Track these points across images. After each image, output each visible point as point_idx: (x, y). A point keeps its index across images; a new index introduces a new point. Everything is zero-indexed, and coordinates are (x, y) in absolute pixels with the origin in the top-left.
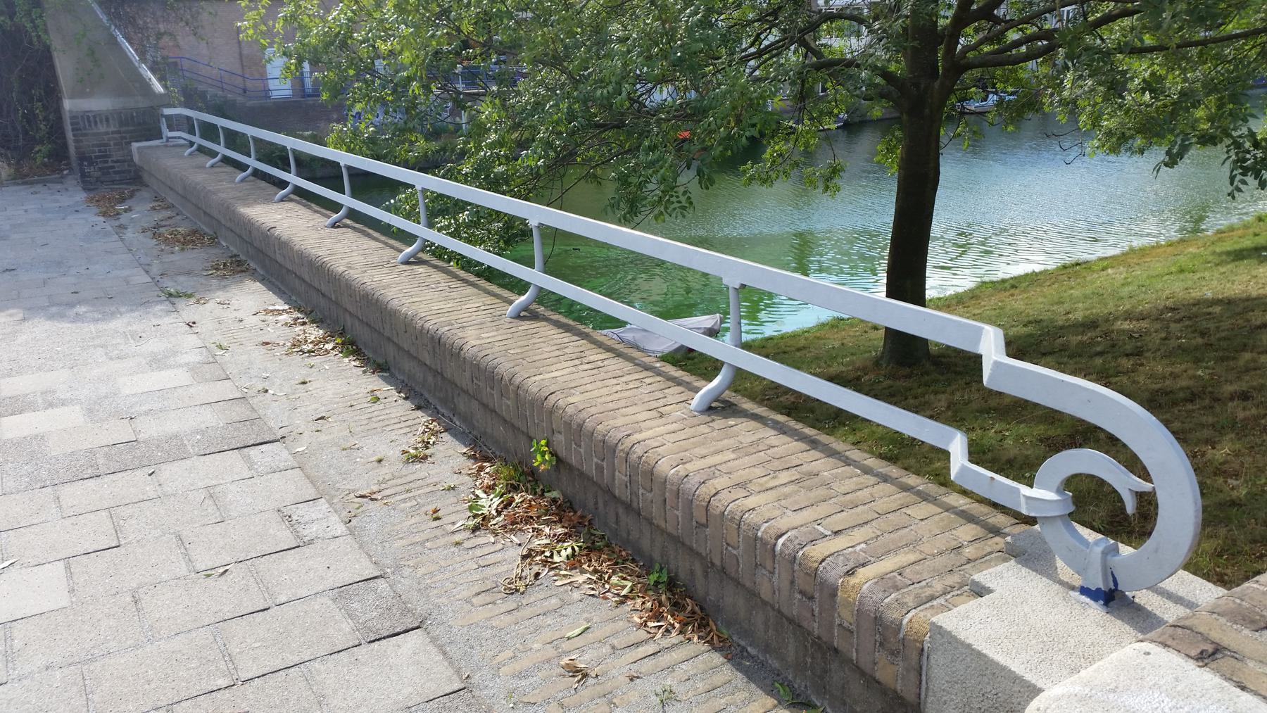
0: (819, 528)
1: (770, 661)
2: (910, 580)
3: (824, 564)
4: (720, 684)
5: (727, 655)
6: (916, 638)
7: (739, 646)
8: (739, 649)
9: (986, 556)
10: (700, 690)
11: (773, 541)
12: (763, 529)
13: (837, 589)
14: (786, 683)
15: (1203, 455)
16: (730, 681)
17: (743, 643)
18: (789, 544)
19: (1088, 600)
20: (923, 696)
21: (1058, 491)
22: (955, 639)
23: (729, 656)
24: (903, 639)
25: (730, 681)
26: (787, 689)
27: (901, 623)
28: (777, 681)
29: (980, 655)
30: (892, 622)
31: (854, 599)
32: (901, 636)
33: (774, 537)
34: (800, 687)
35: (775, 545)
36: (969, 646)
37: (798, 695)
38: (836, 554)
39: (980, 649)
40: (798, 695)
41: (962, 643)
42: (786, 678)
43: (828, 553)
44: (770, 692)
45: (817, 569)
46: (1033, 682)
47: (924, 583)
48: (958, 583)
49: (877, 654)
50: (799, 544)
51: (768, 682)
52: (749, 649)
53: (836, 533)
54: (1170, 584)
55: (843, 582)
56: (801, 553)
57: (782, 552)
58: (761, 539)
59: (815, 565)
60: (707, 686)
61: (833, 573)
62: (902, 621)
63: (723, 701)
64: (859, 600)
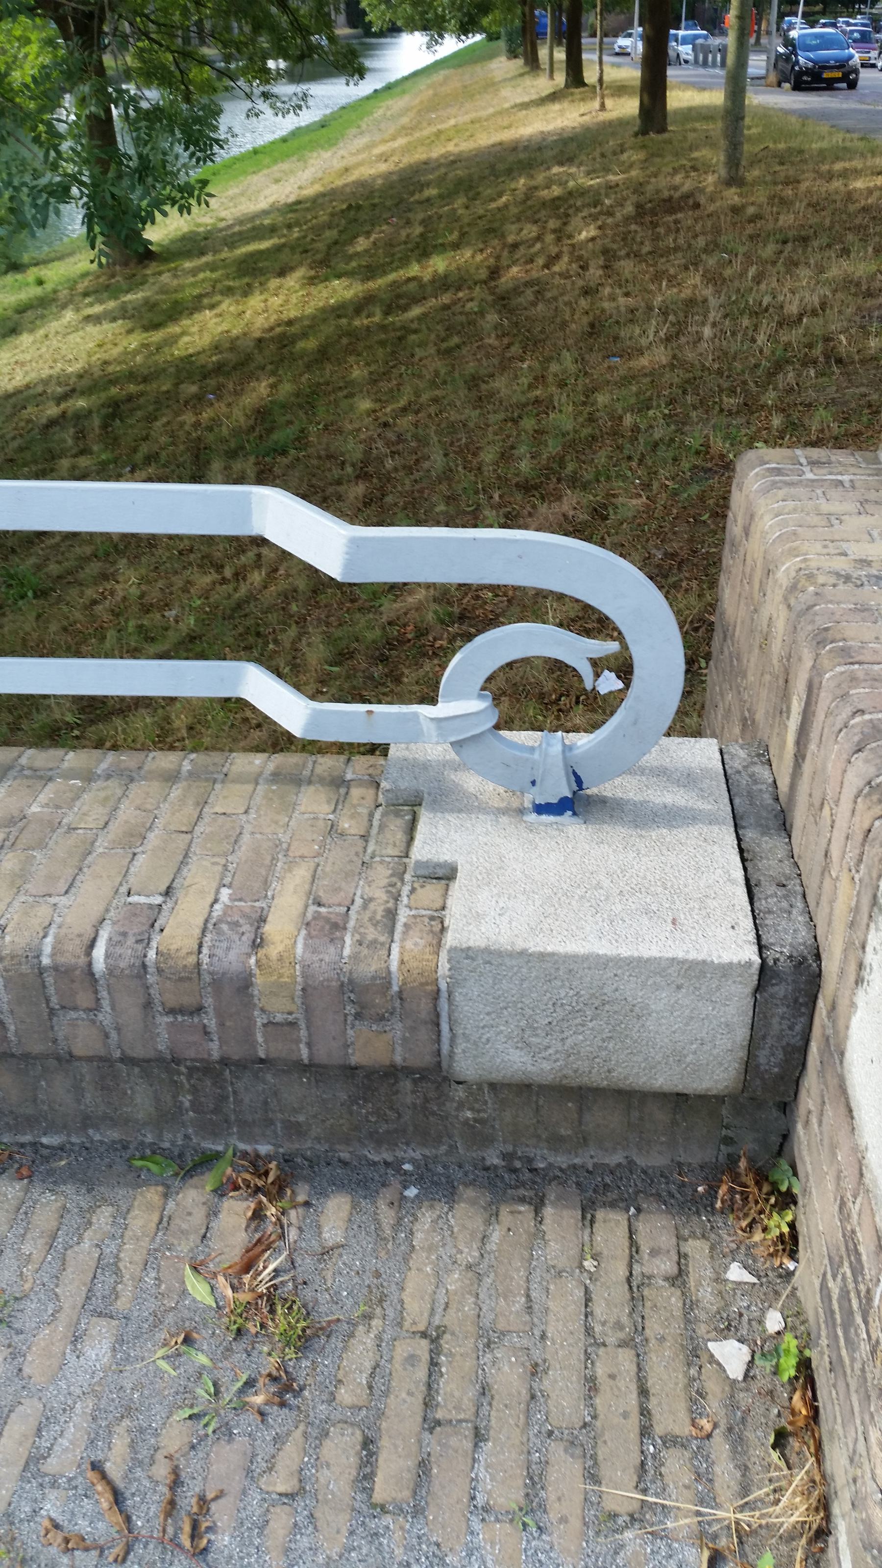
0: (134, 899)
1: (97, 1137)
2: (340, 905)
3: (205, 951)
4: (55, 1224)
5: (18, 1171)
6: (423, 980)
7: (22, 1145)
8: (29, 1150)
9: (371, 821)
10: (37, 1256)
11: (83, 960)
12: (47, 949)
13: (251, 975)
14: (148, 1152)
15: (112, 593)
16: (64, 1207)
17: (27, 1138)
18: (119, 950)
19: (551, 818)
20: (445, 1048)
21: (481, 697)
22: (499, 954)
23: (25, 1172)
24: (400, 992)
25: (64, 1207)
26: (158, 1158)
27: (389, 972)
28: (133, 1157)
29: (543, 957)
30: (374, 978)
31: (294, 976)
32: (395, 988)
33: (80, 952)
34: (173, 1143)
35: (90, 964)
36: (523, 953)
37: (181, 1155)
38: (210, 926)
39: (540, 949)
40: (181, 1155)
41: (511, 955)
42: (142, 1143)
43: (197, 932)
44: (137, 1179)
45: (199, 964)
46: (636, 954)
47: (358, 901)
48: (392, 875)
49: (350, 1032)
50: (137, 942)
51: (120, 1167)
52: (45, 1140)
53: (168, 892)
54: (652, 758)
55: (257, 961)
56: (152, 954)
57: (111, 971)
58: (55, 968)
59: (192, 960)
60: (41, 1241)
61: (232, 956)
62: (388, 968)
63: (86, 1244)
64: (303, 973)
